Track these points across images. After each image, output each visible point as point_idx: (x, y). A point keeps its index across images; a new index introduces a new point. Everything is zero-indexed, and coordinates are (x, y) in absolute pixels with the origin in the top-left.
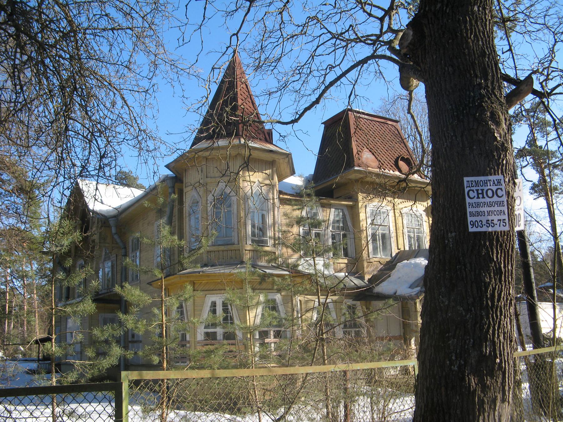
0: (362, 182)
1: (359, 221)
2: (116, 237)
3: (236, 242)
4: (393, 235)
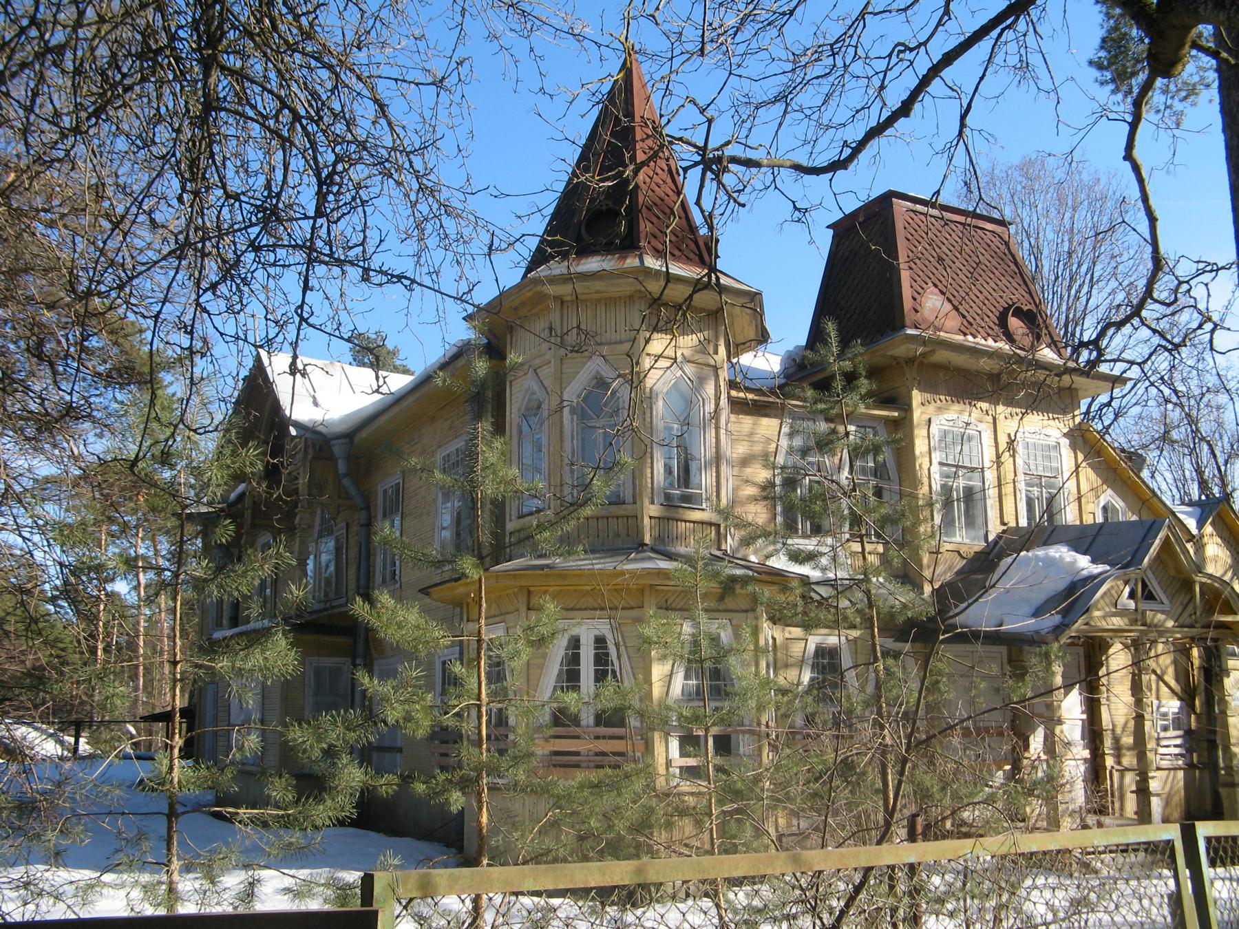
0: (922, 364)
1: (913, 458)
2: (346, 482)
3: (629, 499)
4: (992, 493)
